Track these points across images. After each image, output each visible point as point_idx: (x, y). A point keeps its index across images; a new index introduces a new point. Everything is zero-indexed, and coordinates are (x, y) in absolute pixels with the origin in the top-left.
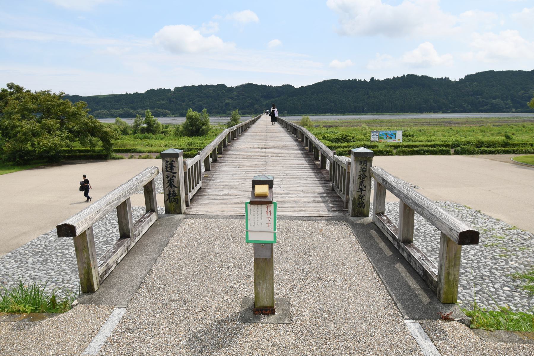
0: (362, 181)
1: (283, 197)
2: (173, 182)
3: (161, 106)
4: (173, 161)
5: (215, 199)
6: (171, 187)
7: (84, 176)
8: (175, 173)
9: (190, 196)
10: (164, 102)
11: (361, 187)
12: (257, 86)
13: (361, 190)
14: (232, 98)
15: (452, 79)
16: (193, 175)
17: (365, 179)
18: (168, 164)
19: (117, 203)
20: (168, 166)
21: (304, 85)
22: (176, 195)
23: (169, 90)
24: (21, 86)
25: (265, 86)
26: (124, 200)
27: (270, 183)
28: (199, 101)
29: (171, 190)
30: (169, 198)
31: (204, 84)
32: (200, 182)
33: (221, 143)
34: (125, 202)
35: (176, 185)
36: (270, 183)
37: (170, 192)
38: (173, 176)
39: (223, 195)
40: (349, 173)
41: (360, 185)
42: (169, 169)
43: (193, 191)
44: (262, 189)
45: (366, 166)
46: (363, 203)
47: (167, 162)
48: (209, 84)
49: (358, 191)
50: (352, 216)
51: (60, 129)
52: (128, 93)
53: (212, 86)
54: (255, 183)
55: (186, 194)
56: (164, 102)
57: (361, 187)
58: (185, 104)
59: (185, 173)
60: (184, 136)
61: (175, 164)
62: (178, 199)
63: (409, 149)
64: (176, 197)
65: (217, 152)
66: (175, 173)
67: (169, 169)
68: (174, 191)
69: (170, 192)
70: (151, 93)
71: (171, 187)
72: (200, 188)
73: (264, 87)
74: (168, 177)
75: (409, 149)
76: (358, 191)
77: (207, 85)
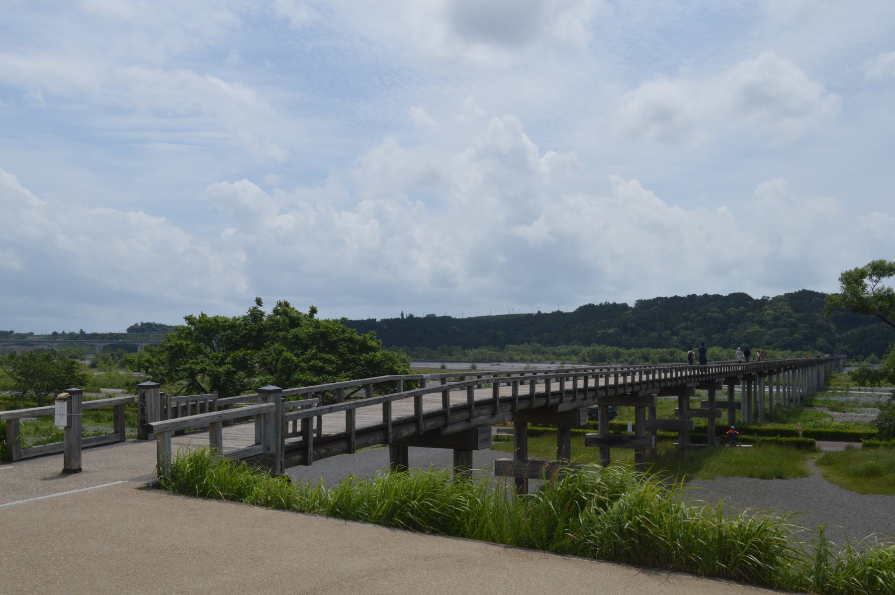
3: (604, 340)
7: (259, 302)
10: (611, 331)
14: (761, 323)
15: (698, 295)
23: (625, 306)
24: (133, 324)
28: (686, 328)
31: (700, 293)
48: (711, 293)
51: (678, 536)
52: (543, 312)
53: (717, 297)
56: (611, 331)
58: (655, 334)
60: (733, 476)
63: (749, 437)
70: (588, 311)
75: (749, 437)
77: (706, 296)
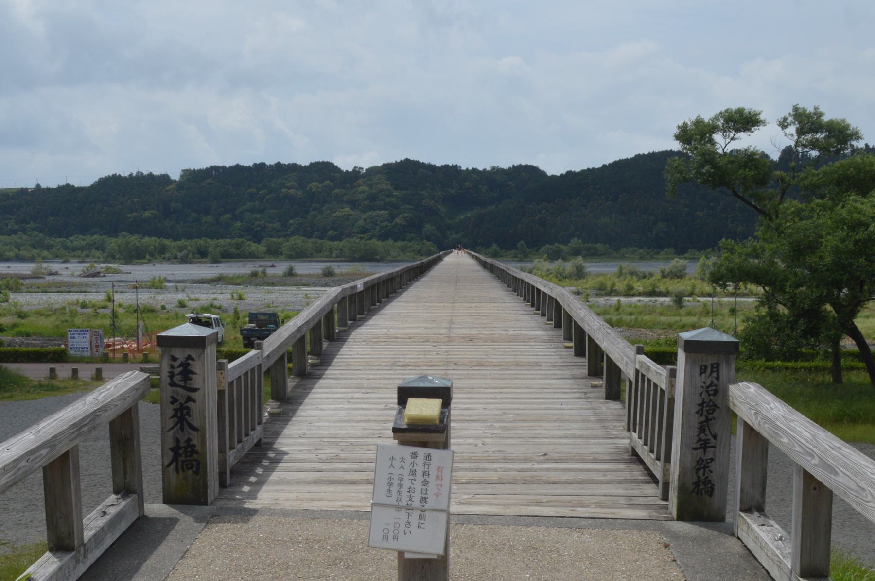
0: (708, 420)
1: (485, 470)
2: (188, 414)
3: (140, 228)
4: (190, 358)
5: (299, 470)
6: (182, 429)
8: (195, 390)
9: (232, 457)
10: (147, 214)
11: (702, 436)
12: (431, 168)
13: (704, 445)
14: (353, 204)
16: (240, 402)
17: (716, 414)
18: (176, 364)
19: (46, 457)
20: (177, 371)
21: (578, 167)
22: (194, 452)
23: (165, 178)
25: (455, 169)
26: (64, 451)
27: (444, 394)
28: (253, 211)
29: (183, 438)
30: (175, 459)
32: (259, 428)
33: (319, 323)
34: (65, 456)
35: (196, 424)
36: (444, 394)
37: (178, 441)
38: (189, 399)
39: (321, 461)
40: (672, 400)
41: (702, 430)
42: (177, 379)
43: (239, 446)
44: (424, 409)
45: (718, 378)
46: (707, 481)
47: (174, 359)
48: (285, 161)
49: (695, 449)
50: (681, 517)
54: (405, 394)
55: (222, 450)
56: (147, 214)
57: (702, 436)
58: (209, 219)
59: (221, 393)
61: (196, 366)
62: (198, 463)
64: (195, 456)
65: (308, 348)
66: (195, 390)
67: (177, 379)
68: (189, 440)
69: (178, 441)
71: (182, 429)
72: (258, 444)
73: (452, 171)
74: (174, 400)
76: (695, 449)
77: (279, 165)
